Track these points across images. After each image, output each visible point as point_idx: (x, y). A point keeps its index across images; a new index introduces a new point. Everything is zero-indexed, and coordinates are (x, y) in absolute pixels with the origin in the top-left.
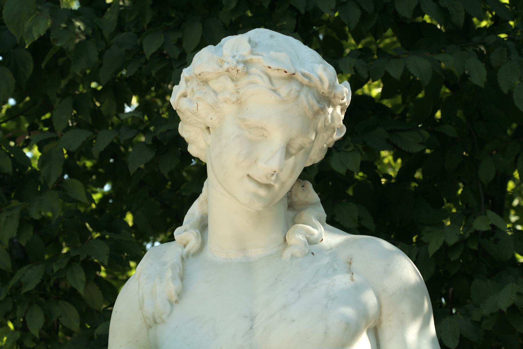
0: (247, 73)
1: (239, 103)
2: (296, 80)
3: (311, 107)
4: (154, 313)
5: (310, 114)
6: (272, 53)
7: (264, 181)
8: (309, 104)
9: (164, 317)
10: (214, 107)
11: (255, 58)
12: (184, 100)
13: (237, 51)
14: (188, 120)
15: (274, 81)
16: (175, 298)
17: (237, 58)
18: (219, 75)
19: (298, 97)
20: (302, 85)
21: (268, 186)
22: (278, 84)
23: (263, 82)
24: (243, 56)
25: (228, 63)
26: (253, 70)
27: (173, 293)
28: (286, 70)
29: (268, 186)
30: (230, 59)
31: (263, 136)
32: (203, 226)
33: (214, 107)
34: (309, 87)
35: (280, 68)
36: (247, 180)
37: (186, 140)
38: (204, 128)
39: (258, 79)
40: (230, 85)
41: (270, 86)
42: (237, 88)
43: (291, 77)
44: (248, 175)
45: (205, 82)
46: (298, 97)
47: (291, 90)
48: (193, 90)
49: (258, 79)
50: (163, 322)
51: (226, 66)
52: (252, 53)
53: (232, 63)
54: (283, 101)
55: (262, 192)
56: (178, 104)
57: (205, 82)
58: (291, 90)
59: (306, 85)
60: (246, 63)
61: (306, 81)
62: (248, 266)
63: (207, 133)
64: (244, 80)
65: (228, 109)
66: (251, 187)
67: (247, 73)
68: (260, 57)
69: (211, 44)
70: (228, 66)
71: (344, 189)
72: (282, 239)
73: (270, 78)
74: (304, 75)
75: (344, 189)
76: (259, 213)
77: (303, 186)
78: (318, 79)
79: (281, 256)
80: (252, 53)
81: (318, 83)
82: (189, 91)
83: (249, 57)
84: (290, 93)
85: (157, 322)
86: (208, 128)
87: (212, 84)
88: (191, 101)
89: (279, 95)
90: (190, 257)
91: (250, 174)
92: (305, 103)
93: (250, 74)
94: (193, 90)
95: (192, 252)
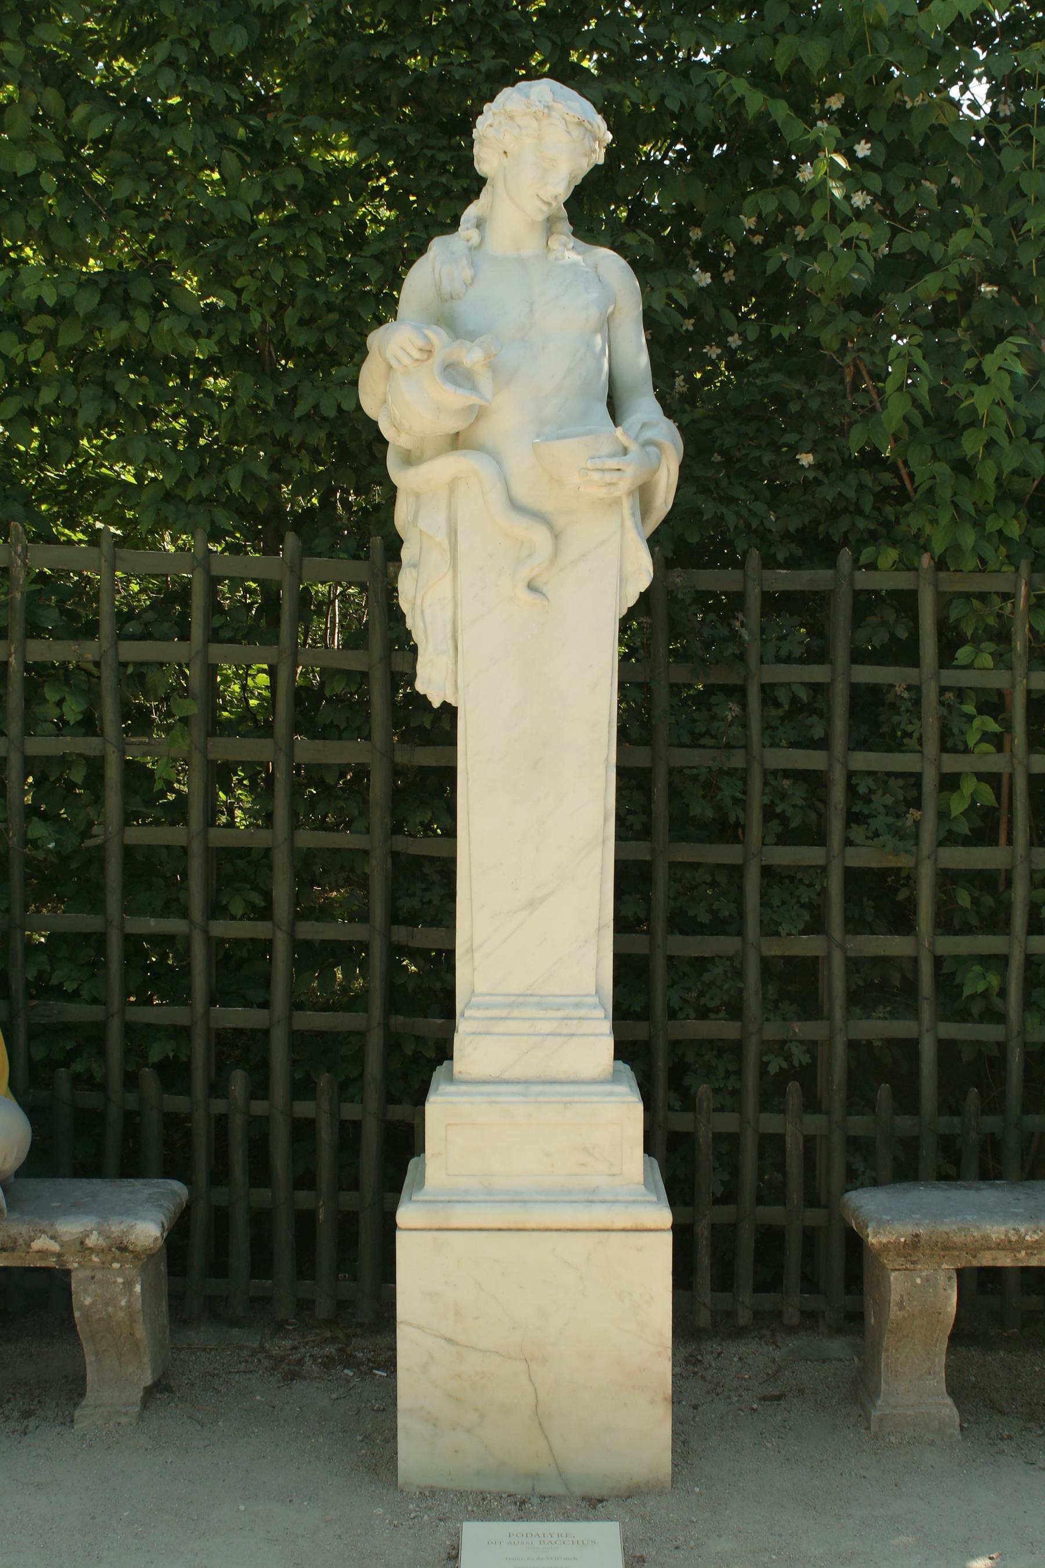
0: (549, 116)
6: (569, 103)
7: (549, 200)
11: (555, 104)
16: (469, 281)
20: (586, 129)
21: (549, 204)
26: (553, 114)
29: (549, 204)
30: (537, 103)
34: (591, 132)
50: (459, 298)
51: (534, 109)
52: (554, 100)
55: (545, 208)
60: (548, 107)
61: (589, 127)
62: (521, 262)
66: (539, 204)
67: (549, 116)
69: (507, 86)
75: (591, 208)
76: (533, 222)
80: (554, 100)
81: (597, 129)
83: (551, 103)
86: (505, 153)
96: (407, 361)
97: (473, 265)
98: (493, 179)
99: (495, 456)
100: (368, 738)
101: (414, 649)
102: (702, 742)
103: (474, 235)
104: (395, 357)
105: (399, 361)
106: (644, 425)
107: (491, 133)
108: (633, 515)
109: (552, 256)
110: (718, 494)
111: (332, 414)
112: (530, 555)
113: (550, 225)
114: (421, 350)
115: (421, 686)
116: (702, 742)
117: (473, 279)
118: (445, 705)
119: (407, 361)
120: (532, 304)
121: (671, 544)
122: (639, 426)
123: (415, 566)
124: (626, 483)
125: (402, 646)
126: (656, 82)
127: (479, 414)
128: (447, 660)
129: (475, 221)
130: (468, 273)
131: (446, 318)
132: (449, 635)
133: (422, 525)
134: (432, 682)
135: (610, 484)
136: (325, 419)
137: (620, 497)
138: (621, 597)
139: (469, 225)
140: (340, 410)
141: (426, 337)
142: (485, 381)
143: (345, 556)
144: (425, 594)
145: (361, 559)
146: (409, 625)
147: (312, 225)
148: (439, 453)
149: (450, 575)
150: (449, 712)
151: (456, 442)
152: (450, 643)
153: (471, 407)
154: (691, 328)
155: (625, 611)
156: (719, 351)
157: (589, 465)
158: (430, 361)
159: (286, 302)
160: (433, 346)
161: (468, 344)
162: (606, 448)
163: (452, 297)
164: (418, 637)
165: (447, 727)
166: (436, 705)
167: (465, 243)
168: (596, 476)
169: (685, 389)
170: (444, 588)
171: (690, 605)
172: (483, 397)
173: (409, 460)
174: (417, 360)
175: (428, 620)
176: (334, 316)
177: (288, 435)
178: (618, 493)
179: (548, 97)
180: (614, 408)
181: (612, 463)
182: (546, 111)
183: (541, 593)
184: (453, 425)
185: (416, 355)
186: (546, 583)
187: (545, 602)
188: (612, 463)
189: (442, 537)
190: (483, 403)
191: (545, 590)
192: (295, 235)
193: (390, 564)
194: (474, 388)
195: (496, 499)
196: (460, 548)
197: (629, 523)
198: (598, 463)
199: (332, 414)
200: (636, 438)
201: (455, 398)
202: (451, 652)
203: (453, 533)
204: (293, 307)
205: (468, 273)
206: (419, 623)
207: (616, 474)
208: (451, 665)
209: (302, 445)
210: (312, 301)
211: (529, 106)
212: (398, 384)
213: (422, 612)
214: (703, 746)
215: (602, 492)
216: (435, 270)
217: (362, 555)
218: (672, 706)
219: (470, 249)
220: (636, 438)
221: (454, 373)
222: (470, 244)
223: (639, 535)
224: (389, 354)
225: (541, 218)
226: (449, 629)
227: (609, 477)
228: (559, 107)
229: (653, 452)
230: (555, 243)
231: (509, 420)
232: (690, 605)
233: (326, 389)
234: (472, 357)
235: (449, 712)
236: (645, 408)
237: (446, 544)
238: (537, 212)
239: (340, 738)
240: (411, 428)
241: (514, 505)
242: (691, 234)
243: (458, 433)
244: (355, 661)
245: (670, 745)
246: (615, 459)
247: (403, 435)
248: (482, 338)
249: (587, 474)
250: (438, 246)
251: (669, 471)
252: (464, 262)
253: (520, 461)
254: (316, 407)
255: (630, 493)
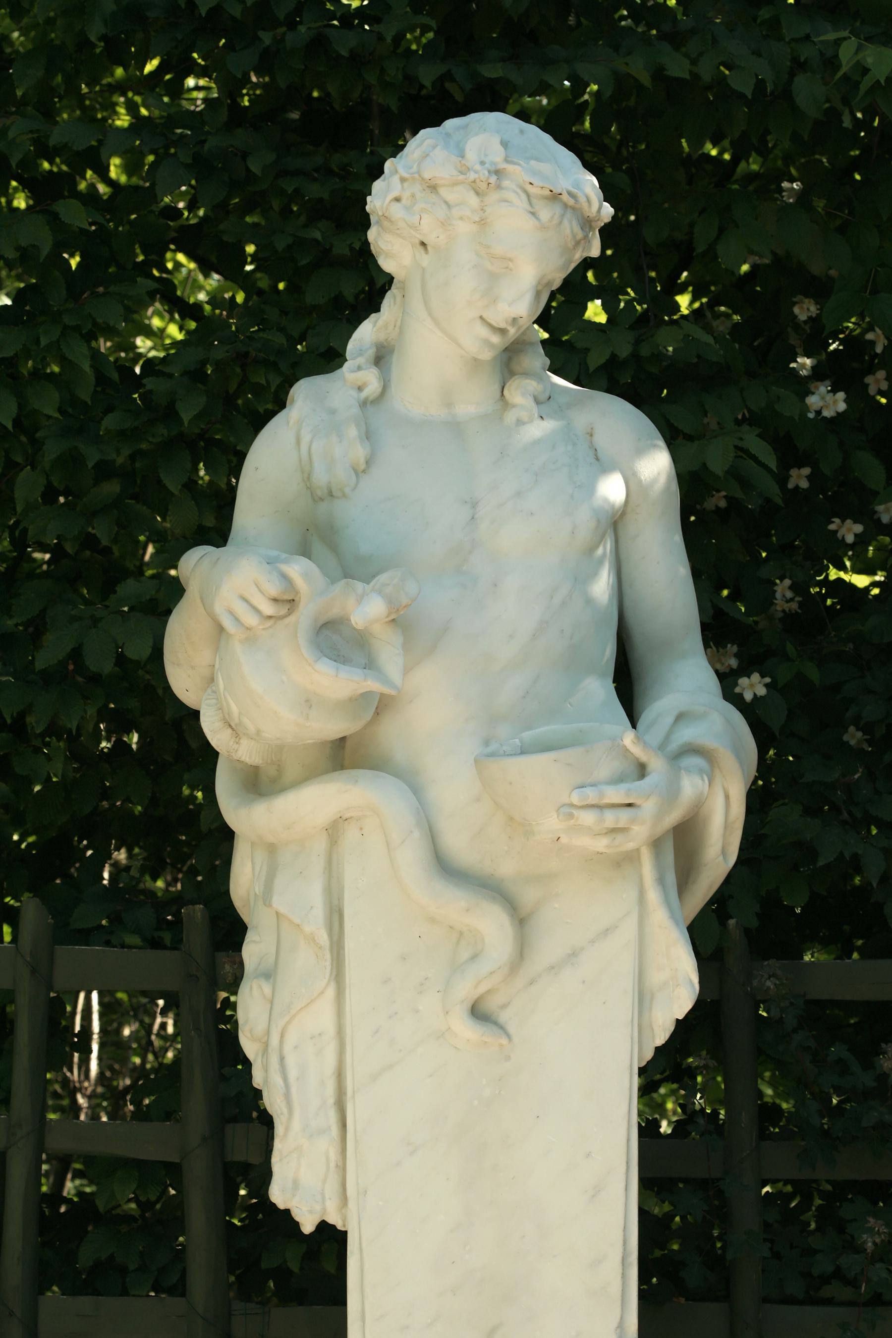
0: (499, 187)
1: (483, 223)
2: (561, 201)
3: (574, 236)
4: (330, 482)
5: (571, 244)
6: (533, 163)
7: (502, 325)
8: (572, 231)
9: (347, 490)
10: (445, 224)
11: (510, 168)
12: (396, 206)
13: (486, 155)
14: (398, 232)
15: (534, 201)
16: (363, 467)
17: (487, 165)
18: (455, 184)
19: (561, 223)
20: (566, 206)
21: (502, 331)
22: (538, 205)
23: (520, 202)
24: (495, 164)
25: (476, 172)
26: (506, 183)
27: (362, 460)
28: (552, 189)
30: (478, 167)
31: (507, 268)
32: (381, 357)
33: (445, 224)
34: (573, 208)
35: (546, 186)
37: (660, 435)
38: (417, 242)
39: (511, 196)
40: (474, 201)
43: (554, 197)
44: (481, 317)
45: (433, 188)
46: (561, 223)
48: (413, 196)
49: (511, 196)
50: (344, 496)
51: (472, 176)
53: (484, 174)
54: (543, 228)
55: (496, 339)
56: (387, 209)
57: (433, 188)
60: (498, 172)
61: (571, 202)
62: (456, 428)
63: (423, 251)
64: (493, 196)
65: (464, 228)
67: (499, 187)
68: (516, 167)
70: (476, 176)
71: (590, 337)
72: (499, 394)
73: (528, 196)
74: (570, 193)
78: (585, 199)
79: (501, 419)
80: (507, 160)
81: (585, 205)
82: (406, 196)
84: (552, 217)
85: (334, 494)
86: (423, 244)
87: (443, 192)
88: (408, 209)
89: (537, 218)
90: (368, 405)
91: (485, 316)
94: (413, 196)
95: (371, 398)
96: (251, 620)
97: (368, 436)
98: (403, 288)
99: (412, 782)
100: (179, 1289)
101: (267, 1121)
102: (827, 1291)
103: (371, 379)
104: (231, 613)
105: (237, 620)
106: (681, 717)
107: (397, 212)
108: (661, 881)
109: (510, 417)
110: (850, 813)
111: (108, 667)
112: (474, 957)
113: (508, 360)
114: (275, 600)
115: (278, 1195)
116: (827, 1291)
117: (368, 463)
118: (324, 1227)
119: (251, 620)
120: (474, 505)
121: (732, 931)
122: (670, 719)
123: (268, 975)
124: (641, 830)
125: (243, 1119)
126: (715, 41)
127: (382, 706)
128: (325, 1147)
129: (371, 352)
130: (360, 453)
131: (317, 534)
132: (331, 1100)
133: (279, 903)
134: (300, 1185)
135: (613, 831)
136: (95, 679)
137: (638, 850)
138: (642, 1028)
139: (361, 360)
140: (121, 660)
141: (284, 577)
142: (390, 654)
143: (136, 940)
144: (286, 1027)
145: (164, 947)
146: (258, 1080)
147: (68, 320)
148: (310, 775)
149: (331, 992)
150: (331, 1240)
151: (342, 755)
152: (332, 1115)
153: (366, 696)
154: (804, 484)
155: (649, 1054)
156: (859, 528)
157: (575, 799)
158: (292, 619)
159: (19, 459)
160: (297, 593)
161: (359, 586)
162: (606, 767)
163: (331, 494)
164: (273, 1102)
165: (331, 1268)
166: (308, 1227)
167: (354, 393)
168: (588, 818)
169: (794, 606)
170: (321, 1017)
171: (795, 1031)
172: (386, 681)
173: (258, 784)
174: (270, 617)
175: (293, 1074)
176: (112, 488)
177: (22, 715)
178: (631, 846)
179: (497, 155)
180: (628, 684)
181: (615, 794)
182: (493, 179)
183: (496, 1023)
184: (334, 727)
185: (268, 609)
186: (504, 1006)
187: (504, 1041)
188: (615, 794)
189: (315, 923)
190: (387, 690)
191: (504, 1017)
192: (38, 342)
193: (221, 957)
194: (370, 665)
195: (411, 857)
196: (350, 944)
197: (653, 896)
198: (591, 796)
199: (108, 667)
200: (662, 747)
201: (335, 682)
202: (335, 1131)
203: (335, 916)
204: (33, 468)
205: (360, 453)
206: (276, 1079)
207: (624, 816)
208: (334, 1155)
209: (54, 730)
210: (72, 461)
211: (464, 170)
212: (237, 651)
213: (282, 1059)
214: (829, 1302)
215: (601, 844)
216: (296, 447)
217: (167, 937)
218: (767, 1225)
219: (364, 404)
220: (662, 747)
221: (336, 639)
222: (364, 395)
223: (673, 916)
224: (219, 608)
225: (487, 355)
226: (330, 1090)
227: (611, 819)
228: (517, 172)
229: (703, 764)
230: (521, 393)
231: (435, 715)
232: (795, 1031)
233: (95, 621)
234: (367, 610)
235: (331, 1240)
236: (688, 683)
237: (323, 938)
238: (479, 343)
239: (124, 1292)
240: (258, 732)
241: (445, 867)
242: (796, 310)
243: (343, 740)
244: (151, 1144)
245: (765, 1300)
246: (624, 786)
247: (244, 742)
248: (383, 578)
249: (571, 816)
250: (305, 394)
251: (727, 797)
252: (353, 432)
253: (453, 786)
254: (76, 654)
255: (656, 844)
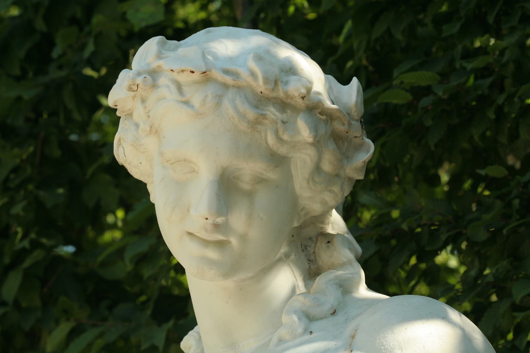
3: (243, 116)
15: (185, 89)
20: (226, 86)
31: (194, 171)
35: (183, 68)
36: (187, 239)
41: (180, 98)
42: (147, 111)
44: (190, 234)
47: (207, 96)
58: (207, 96)
59: (233, 86)
61: (228, 80)
74: (227, 72)
77: (329, 242)
84: (204, 101)
92: (231, 112)
93: (159, 87)
